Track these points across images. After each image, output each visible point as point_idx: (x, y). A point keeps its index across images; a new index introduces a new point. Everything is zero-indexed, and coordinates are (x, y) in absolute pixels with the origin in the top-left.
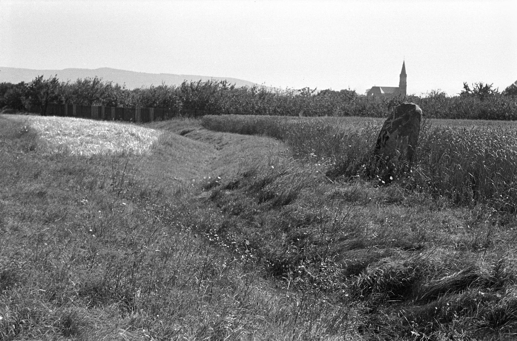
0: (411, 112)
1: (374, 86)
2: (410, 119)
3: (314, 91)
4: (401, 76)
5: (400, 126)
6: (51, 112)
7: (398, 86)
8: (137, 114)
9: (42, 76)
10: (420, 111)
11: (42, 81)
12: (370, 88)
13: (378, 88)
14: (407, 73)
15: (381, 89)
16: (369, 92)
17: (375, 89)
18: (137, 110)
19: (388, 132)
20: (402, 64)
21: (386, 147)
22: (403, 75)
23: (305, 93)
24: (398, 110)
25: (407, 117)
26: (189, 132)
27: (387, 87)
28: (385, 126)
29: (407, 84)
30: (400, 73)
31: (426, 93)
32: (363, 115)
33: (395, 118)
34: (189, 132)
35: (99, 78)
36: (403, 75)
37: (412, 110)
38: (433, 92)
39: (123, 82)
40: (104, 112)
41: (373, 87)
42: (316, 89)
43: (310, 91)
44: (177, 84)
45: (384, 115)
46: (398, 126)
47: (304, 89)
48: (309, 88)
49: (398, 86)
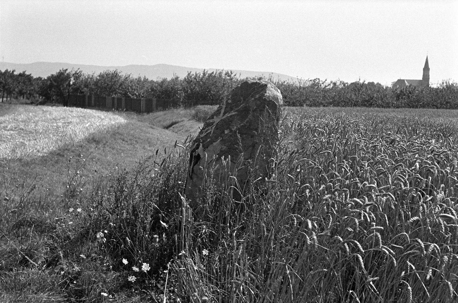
0: (255, 99)
1: (399, 79)
2: (250, 116)
3: (325, 82)
4: (424, 69)
5: (226, 132)
6: (75, 103)
7: (421, 79)
8: (143, 104)
9: (145, 77)
10: (277, 99)
11: (66, 74)
12: (396, 80)
13: (404, 80)
14: (430, 67)
15: (405, 81)
16: (395, 84)
17: (401, 82)
18: (143, 100)
19: (201, 146)
20: (426, 58)
21: (195, 179)
22: (426, 69)
23: (315, 84)
24: (233, 96)
25: (244, 113)
26: (175, 123)
27: (410, 80)
28: (201, 133)
29: (430, 77)
30: (423, 66)
31: (436, 83)
32: (371, 105)
33: (225, 113)
34: (175, 123)
35: (119, 71)
36: (426, 69)
37: (257, 96)
38: (445, 82)
39: (138, 73)
40: (116, 102)
41: (398, 80)
42: (326, 80)
43: (321, 82)
44: (182, 76)
45: (392, 105)
46: (224, 132)
47: (315, 80)
48: (319, 79)
49: (421, 79)
